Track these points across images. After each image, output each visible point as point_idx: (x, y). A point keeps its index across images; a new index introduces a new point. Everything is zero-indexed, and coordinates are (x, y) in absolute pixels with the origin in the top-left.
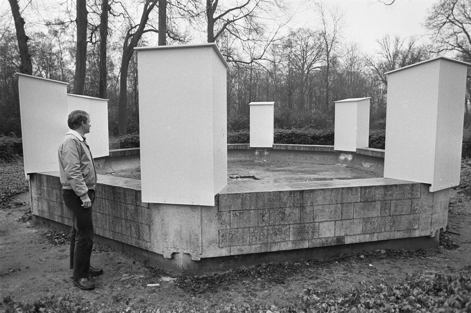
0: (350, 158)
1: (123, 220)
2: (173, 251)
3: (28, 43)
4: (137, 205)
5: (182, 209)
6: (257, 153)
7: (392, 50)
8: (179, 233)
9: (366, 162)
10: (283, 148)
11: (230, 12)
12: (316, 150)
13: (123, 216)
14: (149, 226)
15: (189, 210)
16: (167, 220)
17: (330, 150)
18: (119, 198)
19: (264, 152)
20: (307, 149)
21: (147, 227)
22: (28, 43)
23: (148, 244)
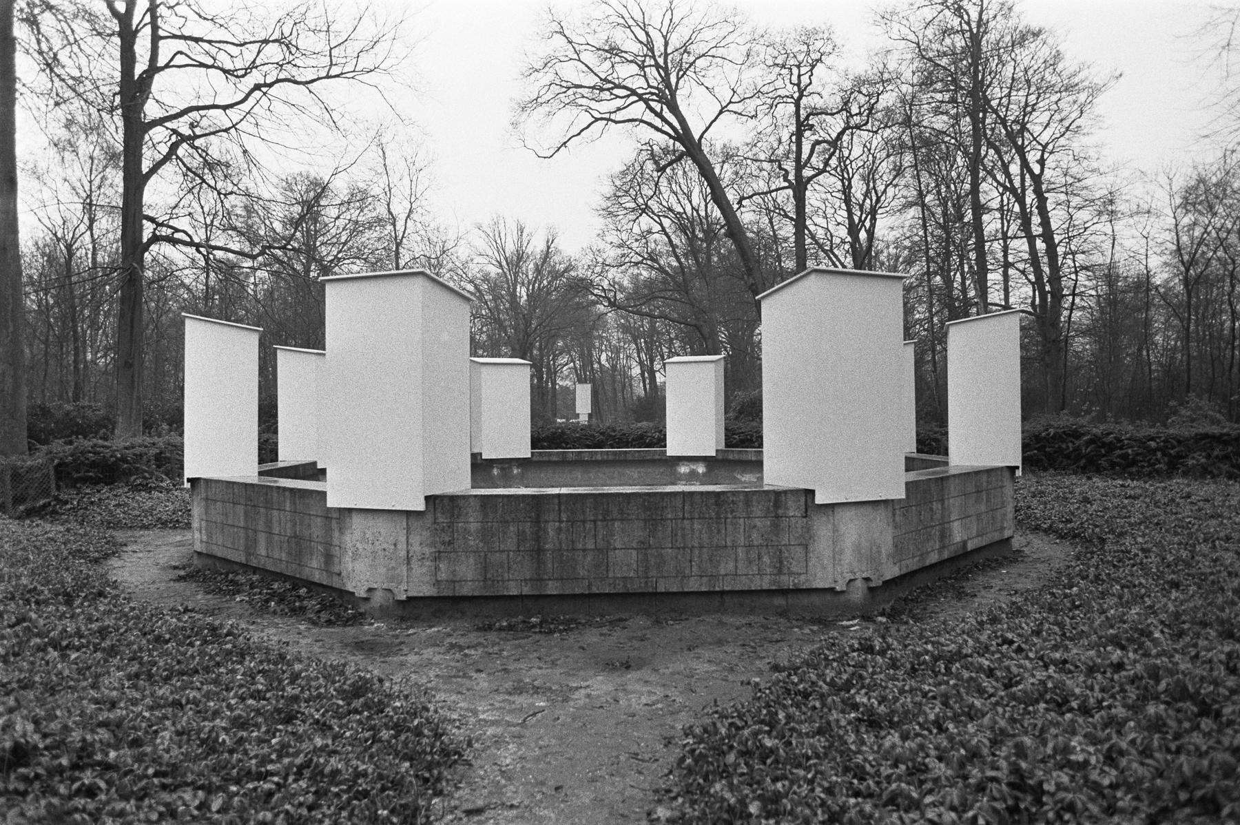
0: (701, 469)
1: (740, 550)
2: (849, 576)
3: (1161, 269)
4: (777, 517)
5: (862, 509)
6: (495, 472)
7: (510, 248)
8: (857, 548)
9: (744, 472)
10: (555, 459)
11: (243, 95)
12: (630, 457)
13: (742, 540)
14: (806, 547)
15: (869, 509)
16: (843, 528)
17: (657, 457)
18: (732, 512)
19: (510, 468)
20: (611, 457)
21: (799, 549)
22: (1161, 269)
23: (803, 578)
